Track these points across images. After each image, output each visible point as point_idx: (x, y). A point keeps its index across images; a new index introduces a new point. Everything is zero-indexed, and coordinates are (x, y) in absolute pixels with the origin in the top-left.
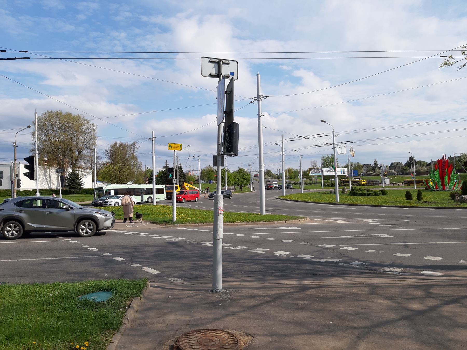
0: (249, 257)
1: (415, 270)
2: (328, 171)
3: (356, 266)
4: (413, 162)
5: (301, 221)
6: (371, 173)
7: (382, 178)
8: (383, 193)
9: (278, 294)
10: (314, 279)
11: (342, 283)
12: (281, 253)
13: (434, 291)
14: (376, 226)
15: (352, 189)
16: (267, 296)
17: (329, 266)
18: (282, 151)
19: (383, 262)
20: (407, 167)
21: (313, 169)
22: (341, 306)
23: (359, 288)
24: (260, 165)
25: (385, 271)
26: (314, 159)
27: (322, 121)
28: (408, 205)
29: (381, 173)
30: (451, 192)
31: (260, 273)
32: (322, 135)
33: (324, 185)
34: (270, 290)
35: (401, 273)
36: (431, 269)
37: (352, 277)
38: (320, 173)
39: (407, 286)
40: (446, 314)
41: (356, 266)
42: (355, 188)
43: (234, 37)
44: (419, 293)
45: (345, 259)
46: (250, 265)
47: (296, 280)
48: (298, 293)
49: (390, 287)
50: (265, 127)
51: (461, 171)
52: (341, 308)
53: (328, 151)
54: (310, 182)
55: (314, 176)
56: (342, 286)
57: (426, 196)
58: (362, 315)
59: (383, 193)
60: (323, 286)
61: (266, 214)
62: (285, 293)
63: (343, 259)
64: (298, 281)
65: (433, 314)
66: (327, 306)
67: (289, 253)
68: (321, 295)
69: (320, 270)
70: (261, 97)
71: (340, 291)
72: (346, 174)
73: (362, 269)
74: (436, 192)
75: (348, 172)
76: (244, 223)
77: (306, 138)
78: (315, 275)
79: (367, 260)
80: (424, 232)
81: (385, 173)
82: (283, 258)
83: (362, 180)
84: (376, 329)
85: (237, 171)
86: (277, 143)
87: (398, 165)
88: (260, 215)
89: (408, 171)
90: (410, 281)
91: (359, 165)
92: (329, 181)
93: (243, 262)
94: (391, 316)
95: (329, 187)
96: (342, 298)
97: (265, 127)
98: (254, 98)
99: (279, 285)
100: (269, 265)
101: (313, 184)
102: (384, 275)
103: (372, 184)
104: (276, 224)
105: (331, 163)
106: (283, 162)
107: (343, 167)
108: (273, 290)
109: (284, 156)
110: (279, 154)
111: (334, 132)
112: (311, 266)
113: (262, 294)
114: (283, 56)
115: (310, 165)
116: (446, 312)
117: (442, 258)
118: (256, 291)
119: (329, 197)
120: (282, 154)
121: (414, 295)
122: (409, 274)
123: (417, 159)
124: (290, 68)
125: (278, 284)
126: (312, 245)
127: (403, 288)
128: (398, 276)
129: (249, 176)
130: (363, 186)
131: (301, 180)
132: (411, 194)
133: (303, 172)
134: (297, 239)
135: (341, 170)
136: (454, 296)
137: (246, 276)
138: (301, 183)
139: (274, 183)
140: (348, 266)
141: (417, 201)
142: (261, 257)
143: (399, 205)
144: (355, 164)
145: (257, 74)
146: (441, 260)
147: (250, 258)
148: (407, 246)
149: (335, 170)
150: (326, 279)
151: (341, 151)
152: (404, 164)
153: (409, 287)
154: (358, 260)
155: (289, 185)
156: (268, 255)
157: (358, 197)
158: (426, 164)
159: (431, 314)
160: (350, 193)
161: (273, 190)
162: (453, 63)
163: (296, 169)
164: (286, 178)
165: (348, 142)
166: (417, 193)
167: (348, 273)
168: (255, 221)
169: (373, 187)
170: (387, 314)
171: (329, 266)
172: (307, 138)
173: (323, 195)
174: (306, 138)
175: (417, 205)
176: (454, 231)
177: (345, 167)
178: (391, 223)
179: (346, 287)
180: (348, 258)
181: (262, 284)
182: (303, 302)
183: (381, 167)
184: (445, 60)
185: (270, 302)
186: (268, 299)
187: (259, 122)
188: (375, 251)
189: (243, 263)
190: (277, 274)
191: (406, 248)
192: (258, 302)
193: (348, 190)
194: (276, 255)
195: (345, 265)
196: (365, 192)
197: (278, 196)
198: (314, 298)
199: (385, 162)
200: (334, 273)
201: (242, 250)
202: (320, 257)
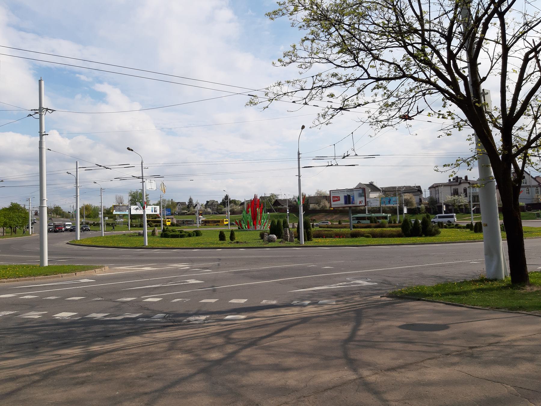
0: (15, 325)
1: (220, 315)
2: (137, 209)
3: (158, 320)
4: (227, 202)
5: (97, 271)
6: (186, 211)
7: (197, 217)
8: (197, 234)
9: (52, 369)
10: (104, 343)
11: (138, 342)
12: (65, 315)
13: (235, 336)
14: (186, 271)
15: (164, 230)
16: (35, 374)
17: (126, 323)
18: (77, 183)
19: (188, 311)
20: (222, 206)
21: (118, 206)
22: (133, 370)
23: (158, 345)
24: (42, 200)
25: (189, 321)
26: (119, 194)
27: (128, 149)
28: (221, 246)
29: (196, 212)
30: (261, 231)
31: (30, 344)
32: (127, 166)
33: (132, 226)
34: (41, 366)
35: (205, 321)
36: (236, 313)
37: (152, 333)
38: (127, 211)
39: (209, 335)
40: (243, 359)
41: (158, 320)
42: (167, 228)
43: (9, 25)
44: (219, 341)
45: (147, 313)
46: (16, 337)
47: (81, 347)
48: (80, 364)
49: (192, 338)
50: (50, 150)
51: (270, 211)
52: (132, 372)
53: (136, 186)
54: (113, 222)
55: (119, 215)
56: (138, 346)
57: (239, 236)
58: (156, 377)
59: (197, 234)
60: (115, 349)
61: (48, 265)
62: (62, 366)
63: (144, 313)
64: (83, 348)
65: (230, 362)
66: (115, 373)
67: (76, 313)
68: (110, 361)
69: (114, 330)
70: (44, 110)
71: (135, 352)
72: (158, 213)
73: (164, 322)
74: (248, 232)
75: (160, 210)
76: (14, 279)
77: (107, 168)
78: (106, 337)
79: (171, 310)
80: (232, 274)
81: (201, 212)
82: (67, 321)
83: (225, 220)
84: (170, 390)
85: (8, 207)
86: (69, 172)
87: (214, 204)
88: (39, 266)
89: (223, 210)
90: (214, 329)
91: (172, 203)
92: (137, 220)
93: (5, 333)
94: (187, 371)
95: (138, 228)
96: (135, 360)
97: (50, 150)
98: (34, 110)
99: (56, 357)
100: (45, 332)
101: (117, 225)
102: (189, 325)
103: (186, 224)
104: (62, 277)
105: (140, 200)
106: (77, 196)
107: (154, 205)
108: (45, 365)
109: (78, 189)
110: (73, 186)
111: (143, 163)
112: (103, 326)
113: (27, 373)
114: (80, 63)
115: (115, 201)
116: (243, 356)
117: (246, 300)
118: (20, 370)
119: (136, 240)
120: (77, 187)
121: (214, 344)
122: (214, 321)
123: (232, 198)
124: (90, 80)
125: (55, 356)
126: (107, 300)
127: (205, 337)
128: (202, 325)
129: (27, 214)
130: (176, 226)
131: (102, 219)
132: (224, 234)
133: (104, 210)
134: (88, 294)
135: (152, 208)
136: (252, 339)
137: (8, 351)
138: (101, 224)
139: (67, 223)
140: (148, 320)
141: (230, 241)
142: (35, 323)
143: (212, 246)
144: (169, 201)
145: (40, 80)
146: (246, 302)
147: (17, 326)
148: (214, 291)
149: (144, 208)
150: (120, 340)
151: (151, 186)
152: (219, 202)
153: (211, 335)
154: (161, 312)
155: (86, 226)
156: (46, 319)
157: (170, 239)
158: (240, 203)
159: (228, 362)
160: (162, 234)
161: (63, 233)
162: (257, 103)
163: (96, 206)
164: (82, 216)
165: (158, 176)
166: (230, 232)
167: (147, 329)
168: (30, 276)
169: (187, 227)
170: (183, 370)
171: (126, 323)
172: (108, 168)
173: (129, 238)
174: (107, 168)
175: (229, 246)
176: (261, 271)
177: (157, 205)
178: (202, 267)
179: (143, 346)
180: (150, 312)
181: (31, 360)
182: (85, 374)
183: (196, 205)
184: (250, 99)
185: (39, 381)
186: (37, 378)
187: (41, 143)
188: (181, 299)
189: (5, 334)
190: (55, 343)
191: (213, 292)
192: (20, 385)
193: (159, 231)
194: (57, 318)
195: (145, 320)
196: (178, 233)
197: (70, 241)
198: (99, 367)
199: (201, 200)
200: (131, 331)
201: (7, 316)
202: (115, 314)
